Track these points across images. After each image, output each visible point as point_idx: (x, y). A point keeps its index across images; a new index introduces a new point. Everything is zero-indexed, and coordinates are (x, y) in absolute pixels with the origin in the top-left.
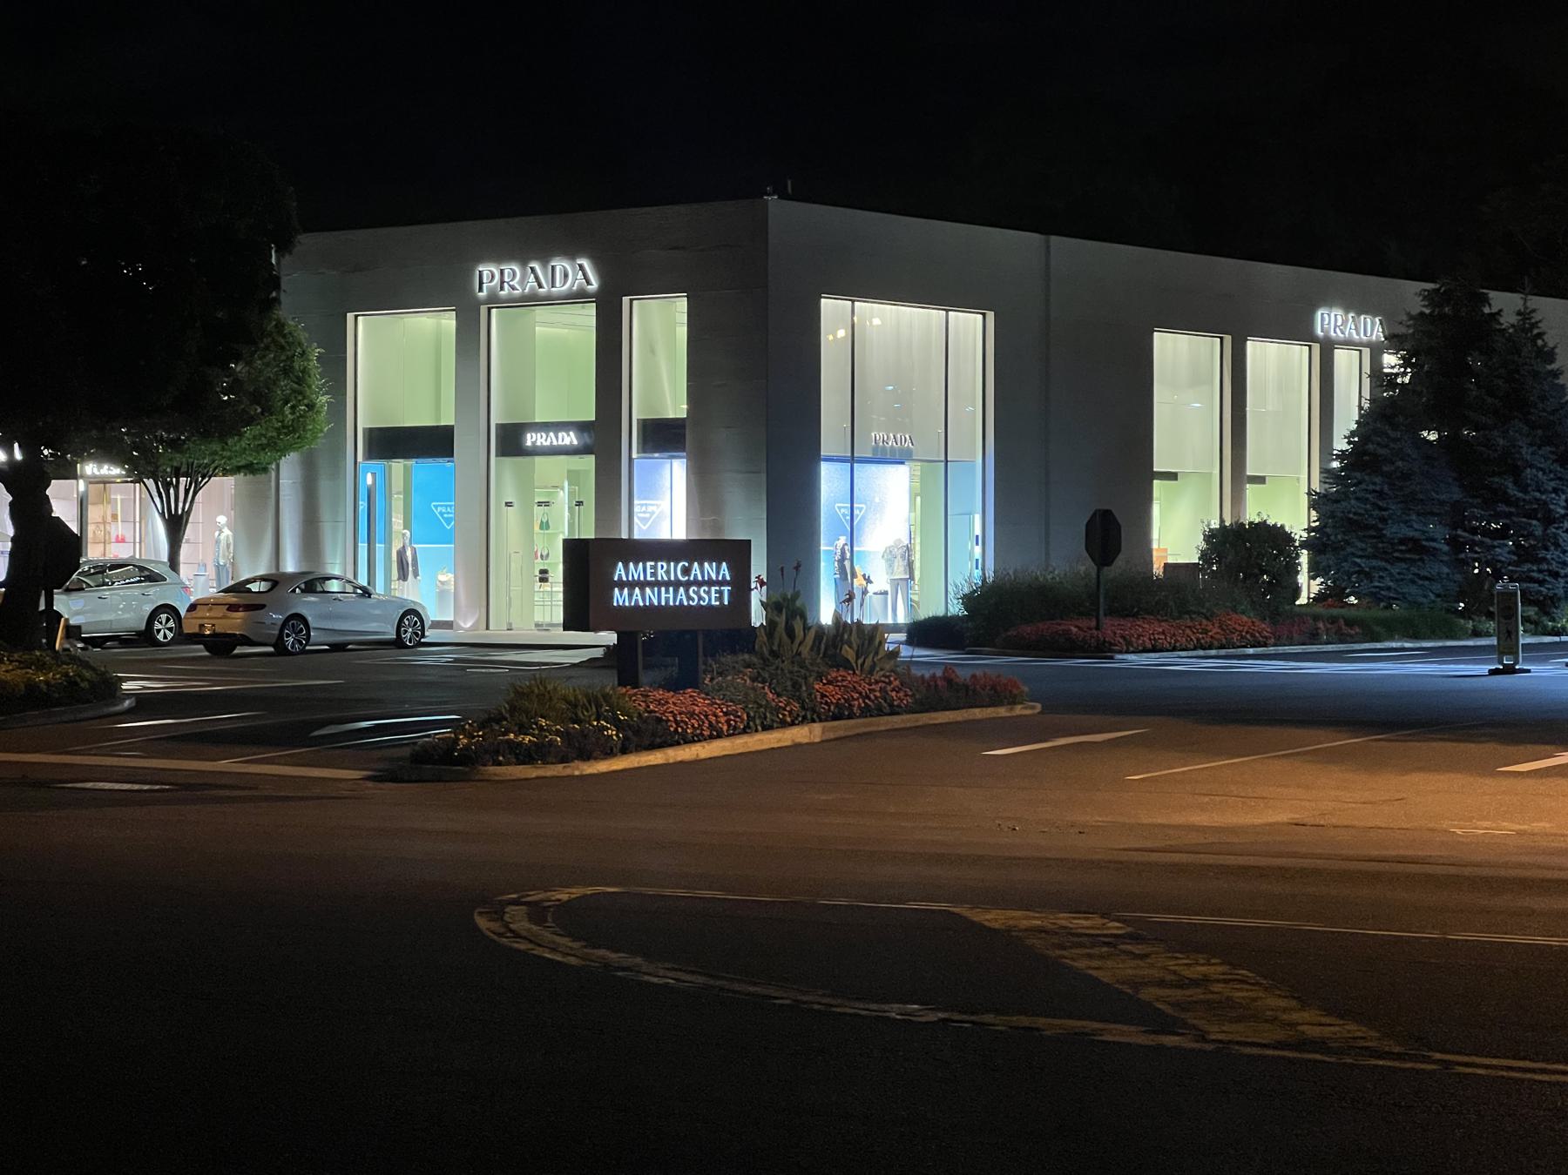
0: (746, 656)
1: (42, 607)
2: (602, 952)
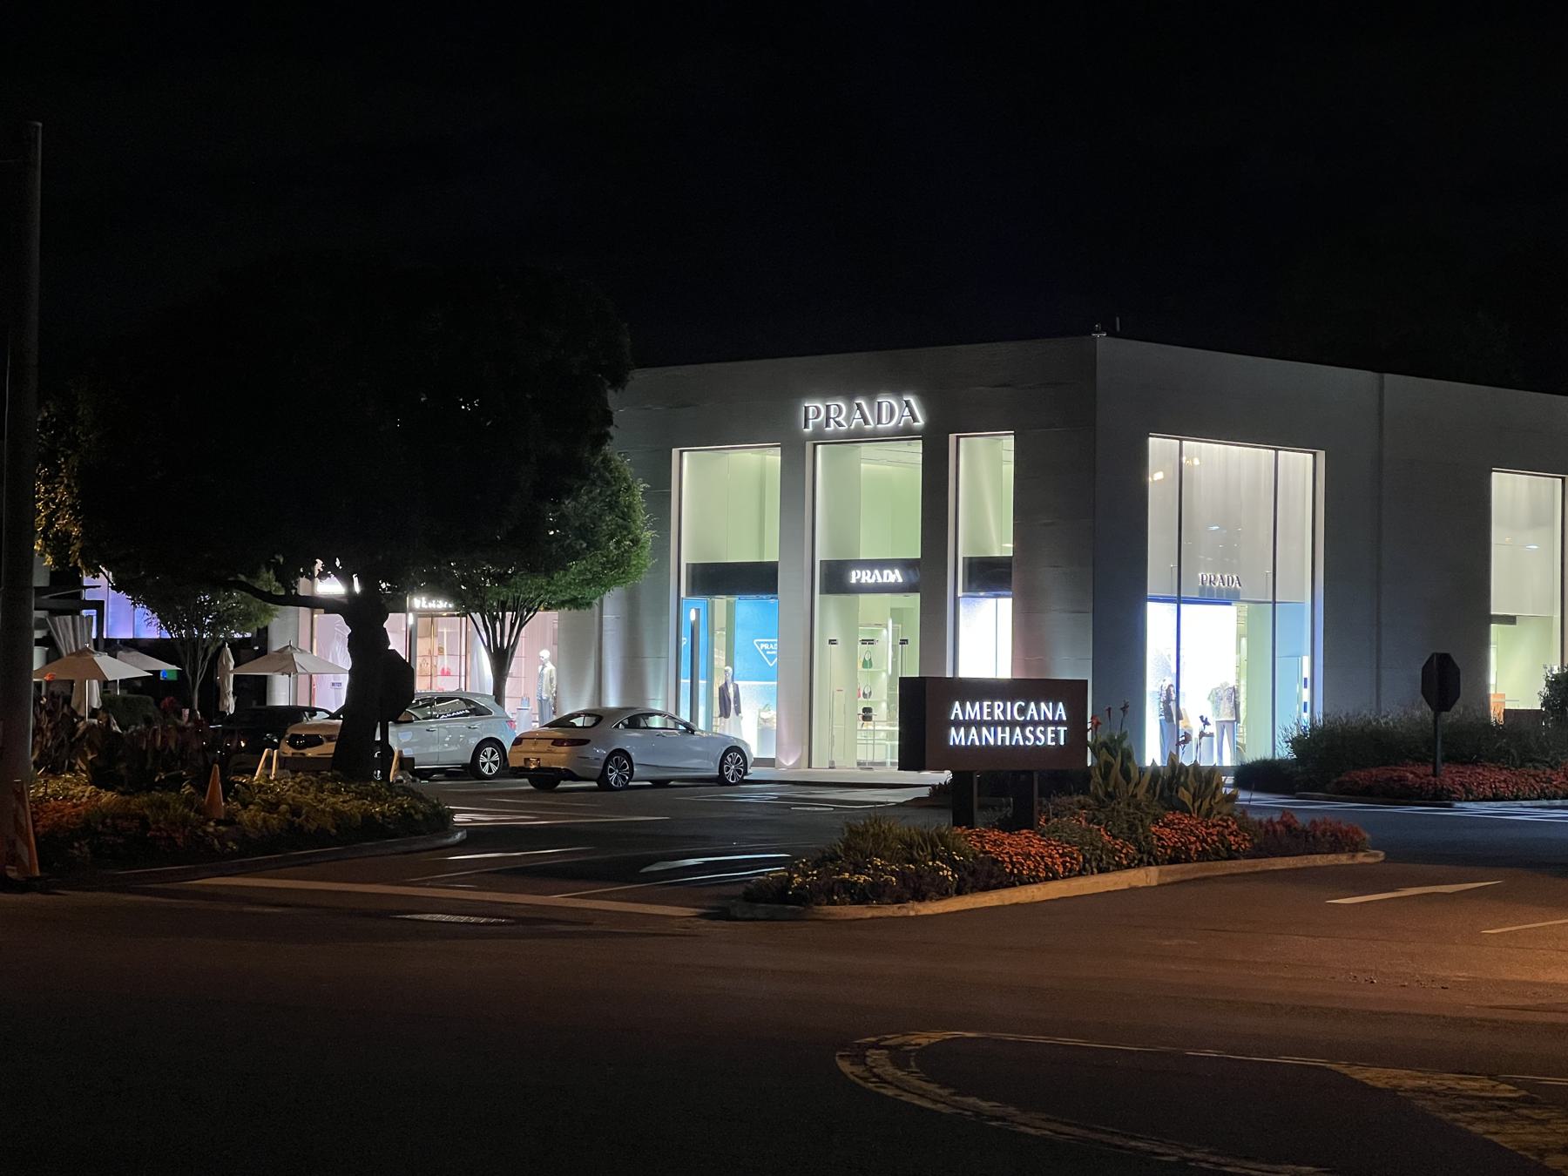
0: (1081, 797)
1: (378, 738)
2: (971, 1100)
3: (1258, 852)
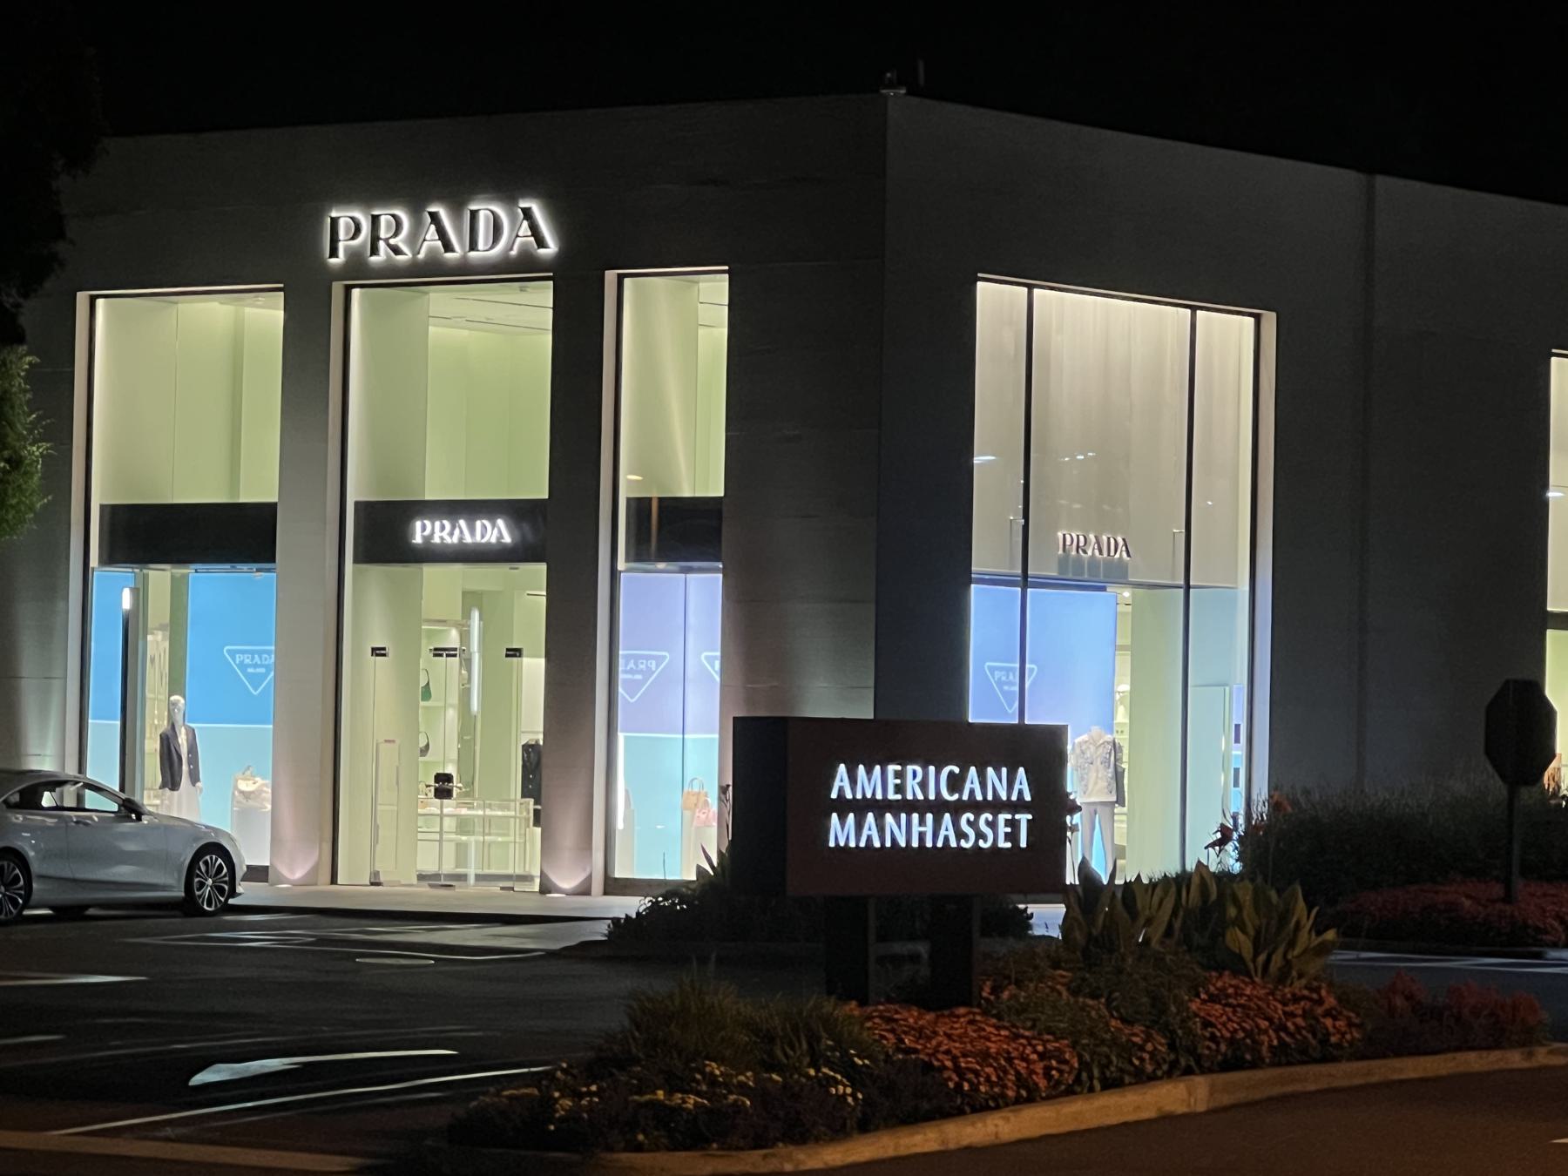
3: (1372, 1049)
